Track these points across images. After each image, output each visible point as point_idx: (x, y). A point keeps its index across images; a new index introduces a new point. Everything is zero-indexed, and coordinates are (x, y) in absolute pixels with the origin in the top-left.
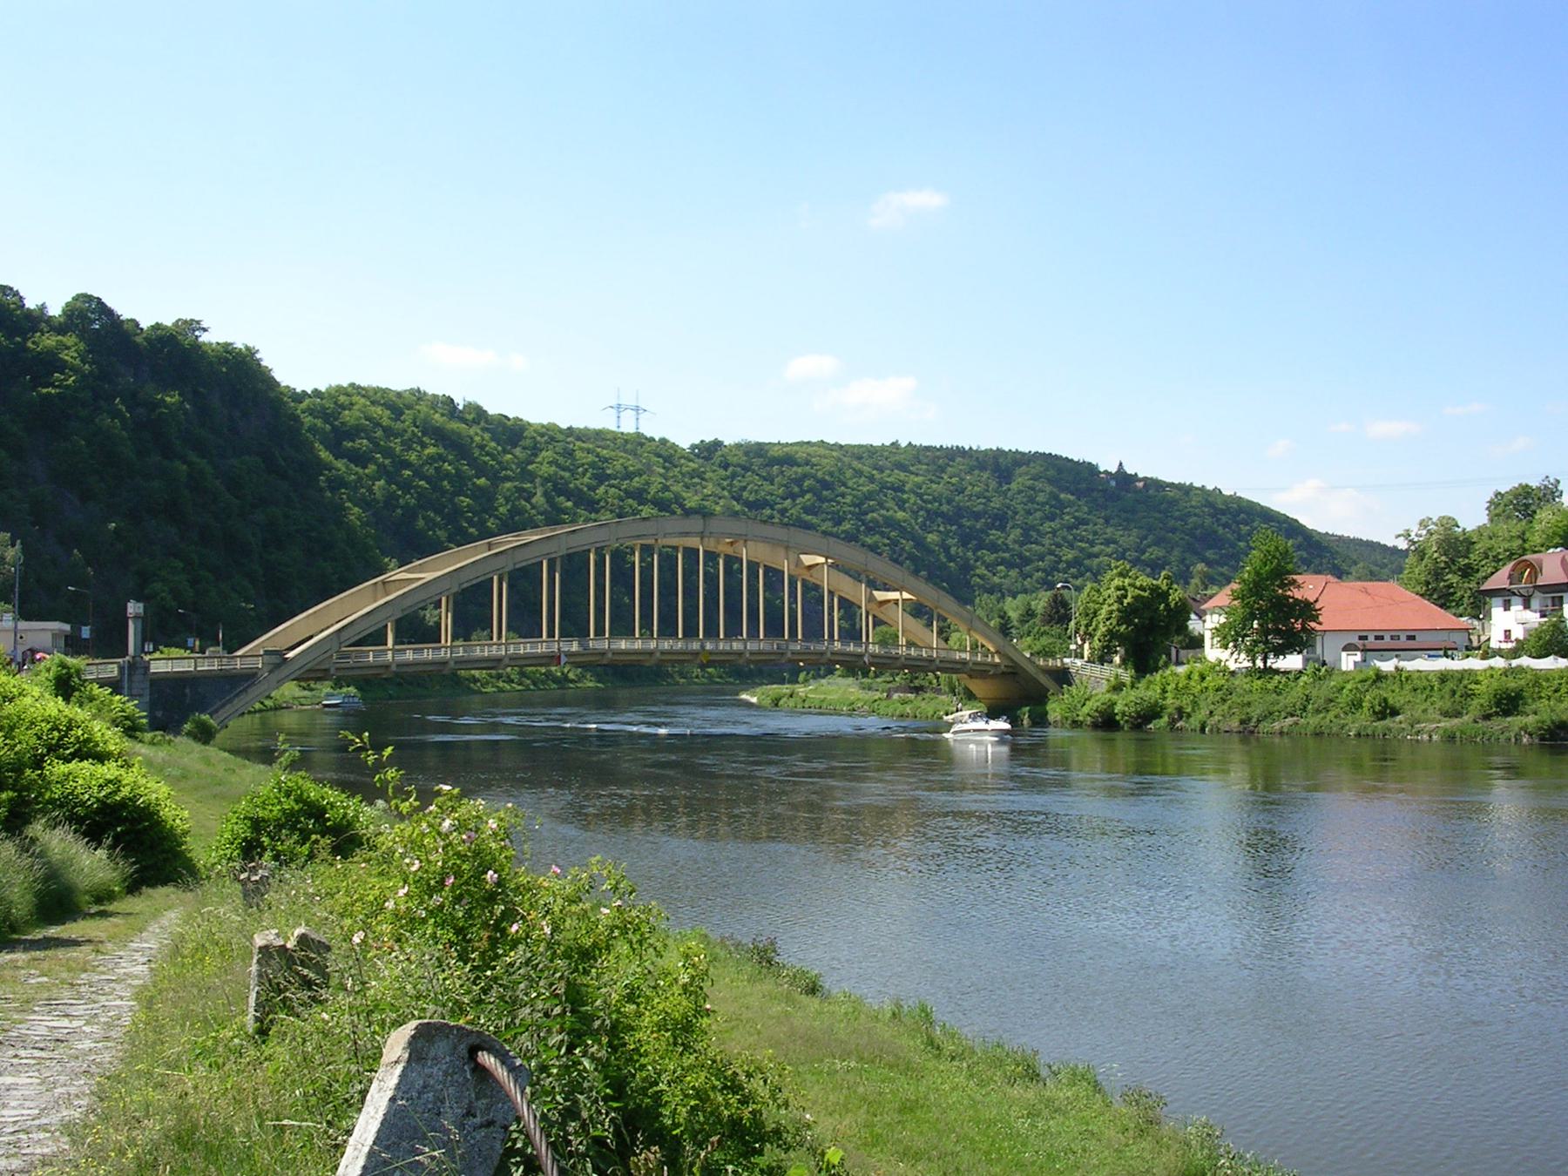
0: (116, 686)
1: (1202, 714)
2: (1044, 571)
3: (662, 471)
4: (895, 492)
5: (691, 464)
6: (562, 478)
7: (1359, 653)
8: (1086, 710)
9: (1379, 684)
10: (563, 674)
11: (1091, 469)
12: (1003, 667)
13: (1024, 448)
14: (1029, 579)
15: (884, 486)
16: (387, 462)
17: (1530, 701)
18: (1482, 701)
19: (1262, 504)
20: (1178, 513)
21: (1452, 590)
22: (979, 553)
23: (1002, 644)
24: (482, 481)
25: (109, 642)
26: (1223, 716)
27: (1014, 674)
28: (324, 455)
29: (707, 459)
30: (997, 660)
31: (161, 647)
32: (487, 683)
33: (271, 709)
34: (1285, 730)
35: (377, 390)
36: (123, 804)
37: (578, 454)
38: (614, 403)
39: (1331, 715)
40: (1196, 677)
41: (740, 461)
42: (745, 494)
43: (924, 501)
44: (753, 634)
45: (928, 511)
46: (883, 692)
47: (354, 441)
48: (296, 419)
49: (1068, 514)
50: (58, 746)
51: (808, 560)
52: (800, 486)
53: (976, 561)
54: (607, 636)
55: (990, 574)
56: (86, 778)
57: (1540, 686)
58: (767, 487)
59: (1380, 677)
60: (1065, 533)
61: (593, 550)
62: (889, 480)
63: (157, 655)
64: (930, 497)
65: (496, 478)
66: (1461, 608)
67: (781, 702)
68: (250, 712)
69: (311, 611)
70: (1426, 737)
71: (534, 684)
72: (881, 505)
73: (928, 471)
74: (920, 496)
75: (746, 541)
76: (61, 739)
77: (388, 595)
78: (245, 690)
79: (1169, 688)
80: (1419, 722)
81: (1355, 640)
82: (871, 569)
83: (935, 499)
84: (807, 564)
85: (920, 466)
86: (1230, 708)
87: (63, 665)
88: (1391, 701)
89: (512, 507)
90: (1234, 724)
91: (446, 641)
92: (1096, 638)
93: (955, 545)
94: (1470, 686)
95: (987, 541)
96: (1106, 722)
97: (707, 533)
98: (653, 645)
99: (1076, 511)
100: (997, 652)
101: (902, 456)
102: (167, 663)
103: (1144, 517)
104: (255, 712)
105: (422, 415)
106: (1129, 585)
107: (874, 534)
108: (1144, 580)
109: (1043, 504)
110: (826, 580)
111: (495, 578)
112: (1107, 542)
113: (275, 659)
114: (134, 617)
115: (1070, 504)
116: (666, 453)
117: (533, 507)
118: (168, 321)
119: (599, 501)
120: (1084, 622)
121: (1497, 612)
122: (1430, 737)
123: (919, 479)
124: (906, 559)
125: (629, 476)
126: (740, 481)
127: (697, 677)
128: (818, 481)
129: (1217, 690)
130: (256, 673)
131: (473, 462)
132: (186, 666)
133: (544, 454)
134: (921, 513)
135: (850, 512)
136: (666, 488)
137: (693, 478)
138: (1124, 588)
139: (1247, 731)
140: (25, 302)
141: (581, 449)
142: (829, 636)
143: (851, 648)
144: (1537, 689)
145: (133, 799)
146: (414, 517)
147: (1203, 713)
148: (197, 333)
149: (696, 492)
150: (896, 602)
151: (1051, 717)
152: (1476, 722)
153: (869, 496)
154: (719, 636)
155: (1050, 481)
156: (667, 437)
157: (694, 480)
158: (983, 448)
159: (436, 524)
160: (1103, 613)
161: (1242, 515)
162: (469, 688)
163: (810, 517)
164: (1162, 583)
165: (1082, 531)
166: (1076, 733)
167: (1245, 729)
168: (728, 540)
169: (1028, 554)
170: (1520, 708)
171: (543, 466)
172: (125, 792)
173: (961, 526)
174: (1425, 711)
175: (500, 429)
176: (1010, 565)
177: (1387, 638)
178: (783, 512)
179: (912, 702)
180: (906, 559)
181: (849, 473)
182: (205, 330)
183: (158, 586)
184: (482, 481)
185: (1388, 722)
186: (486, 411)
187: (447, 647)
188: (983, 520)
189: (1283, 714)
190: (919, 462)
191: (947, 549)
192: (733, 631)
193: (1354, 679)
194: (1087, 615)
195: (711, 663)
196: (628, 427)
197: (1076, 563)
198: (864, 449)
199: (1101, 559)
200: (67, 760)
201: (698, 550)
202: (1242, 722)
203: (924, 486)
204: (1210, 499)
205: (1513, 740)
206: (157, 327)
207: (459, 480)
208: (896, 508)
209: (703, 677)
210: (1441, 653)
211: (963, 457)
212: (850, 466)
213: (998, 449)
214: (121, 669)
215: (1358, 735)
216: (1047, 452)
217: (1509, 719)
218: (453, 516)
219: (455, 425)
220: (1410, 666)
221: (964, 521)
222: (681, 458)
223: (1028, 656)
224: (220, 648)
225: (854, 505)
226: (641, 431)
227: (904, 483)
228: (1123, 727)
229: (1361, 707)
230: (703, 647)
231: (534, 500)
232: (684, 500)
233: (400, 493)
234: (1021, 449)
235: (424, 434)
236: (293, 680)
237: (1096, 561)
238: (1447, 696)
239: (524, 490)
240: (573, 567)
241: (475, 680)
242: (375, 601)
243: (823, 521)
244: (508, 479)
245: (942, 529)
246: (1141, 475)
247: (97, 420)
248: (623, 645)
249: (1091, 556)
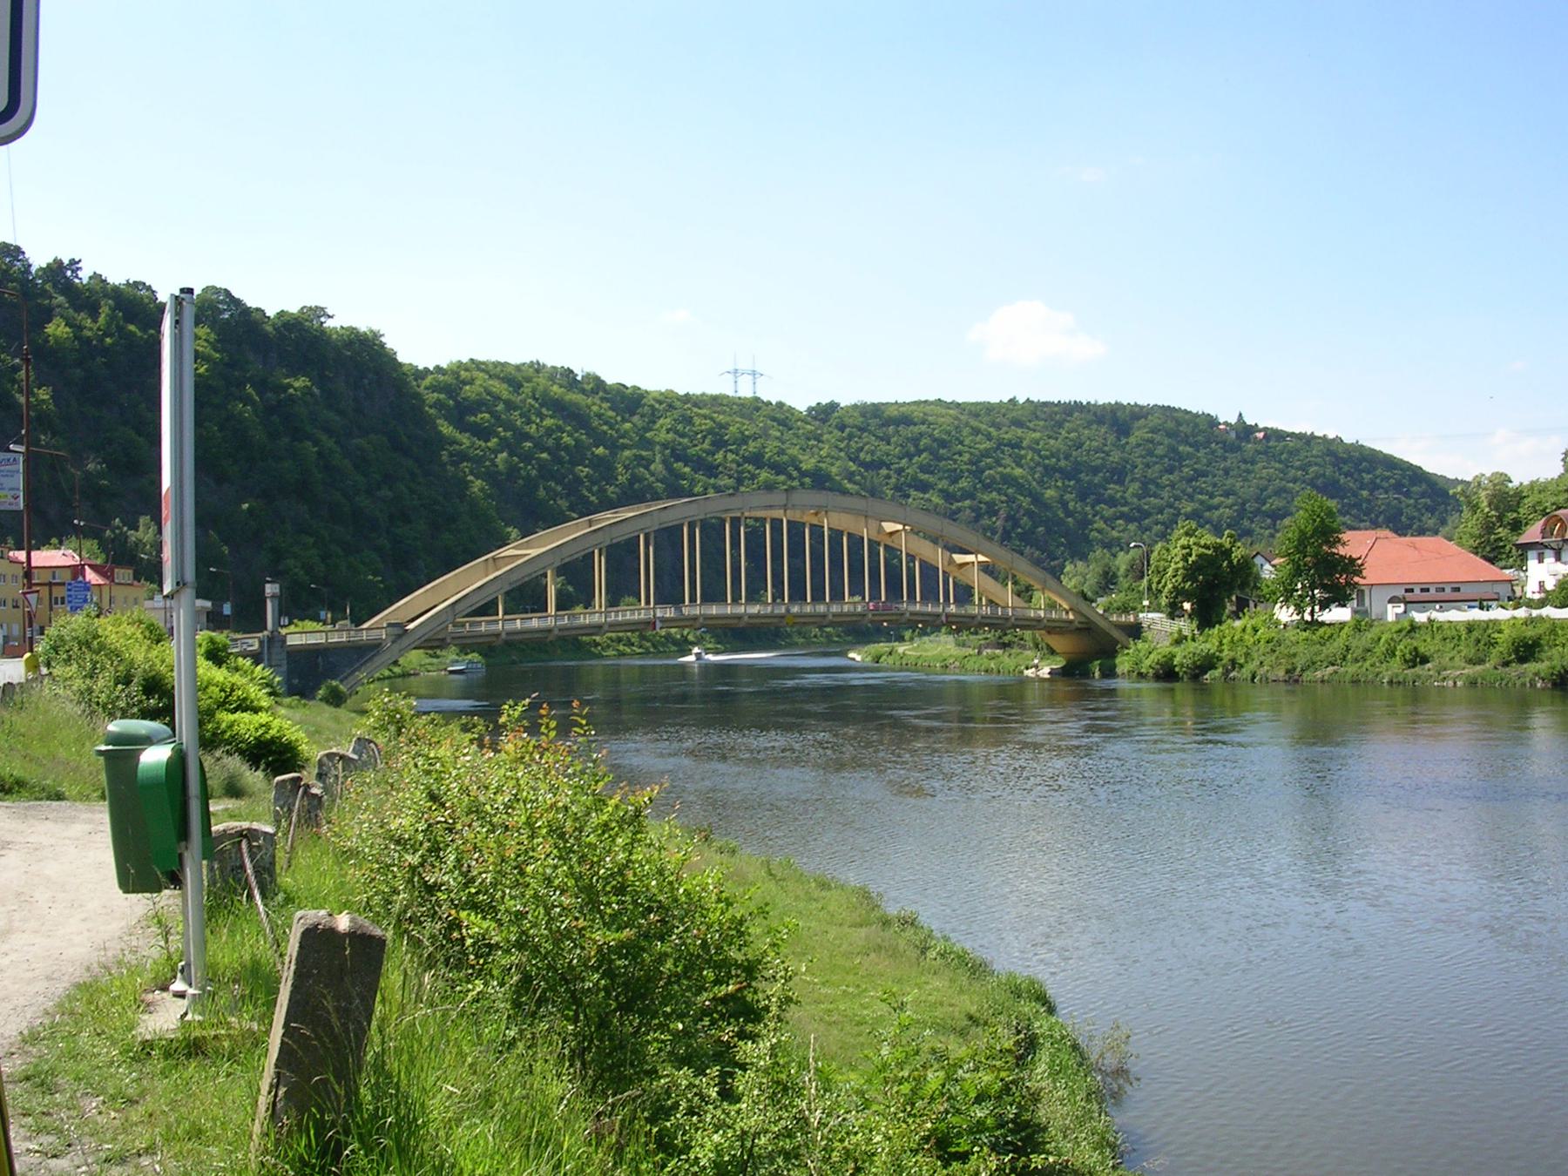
0: (257, 658)
1: (1252, 666)
2: (1163, 523)
3: (778, 434)
5: (809, 427)
6: (680, 444)
7: (1402, 605)
8: (1147, 662)
9: (1413, 634)
10: (682, 636)
11: (1212, 422)
13: (1143, 401)
14: (1148, 533)
15: (1000, 444)
16: (509, 434)
17: (1546, 648)
18: (1501, 649)
19: (1385, 451)
20: (1298, 463)
21: (1501, 544)
22: (1098, 508)
23: (1075, 601)
24: (600, 450)
25: (249, 618)
26: (1271, 666)
27: (1088, 629)
28: (446, 429)
29: (824, 421)
30: (1071, 617)
31: (295, 621)
32: (608, 646)
33: (399, 676)
34: (1326, 678)
35: (497, 364)
36: (273, 740)
37: (697, 421)
38: (731, 369)
39: (1368, 664)
40: (1249, 630)
41: (856, 422)
42: (862, 455)
43: (1041, 457)
44: (736, 599)
45: (1046, 467)
46: (974, 648)
47: (476, 416)
48: (417, 396)
49: (1187, 466)
50: (224, 703)
51: (889, 527)
52: (916, 446)
53: (1094, 516)
54: (698, 602)
55: (1110, 529)
56: (247, 725)
57: (1556, 634)
58: (884, 447)
59: (1414, 628)
60: (1184, 485)
62: (1006, 436)
63: (292, 628)
64: (1048, 453)
65: (614, 447)
66: (1511, 560)
67: (881, 660)
68: (379, 679)
69: (457, 571)
70: (1451, 683)
71: (654, 646)
72: (998, 463)
73: (1045, 427)
74: (1038, 452)
75: (826, 512)
76: (227, 697)
77: (497, 570)
78: (371, 659)
79: (1225, 641)
80: (1445, 670)
81: (1400, 592)
83: (1052, 455)
84: (888, 530)
85: (1037, 422)
86: (1277, 658)
87: (212, 641)
88: (1422, 650)
89: (631, 475)
90: (1281, 673)
91: (601, 607)
92: (1163, 595)
93: (1073, 500)
94: (1493, 636)
95: (1106, 496)
96: (1167, 673)
97: (790, 506)
98: (741, 610)
99: (1195, 463)
100: (1071, 609)
101: (1020, 412)
102: (302, 635)
103: (1264, 468)
104: (384, 679)
105: (541, 388)
106: (1195, 544)
107: (991, 492)
108: (1209, 539)
109: (1162, 457)
110: (903, 544)
111: (596, 551)
112: (1227, 494)
113: (397, 631)
114: (272, 597)
115: (1189, 456)
116: (781, 416)
117: (652, 475)
118: (293, 309)
119: (718, 466)
120: (1156, 580)
121: (1532, 563)
122: (1455, 683)
123: (1037, 435)
124: (1024, 515)
125: (744, 440)
126: (856, 442)
127: (815, 636)
128: (935, 440)
129: (1268, 642)
130: (380, 644)
131: (591, 432)
132: (312, 640)
133: (661, 421)
134: (1039, 469)
136: (782, 452)
137: (809, 439)
138: (1189, 547)
139: (1292, 678)
140: (158, 296)
141: (698, 415)
142: (944, 601)
144: (1552, 637)
145: (280, 738)
146: (536, 487)
147: (1252, 666)
148: (323, 319)
149: (813, 455)
151: (1119, 670)
152: (1496, 668)
153: (986, 454)
154: (806, 600)
155: (1169, 434)
156: (783, 400)
157: (810, 443)
158: (1100, 403)
159: (556, 494)
160: (1170, 572)
161: (1364, 464)
162: (590, 651)
163: (927, 476)
164: (1225, 541)
165: (1201, 483)
166: (1143, 685)
167: (1290, 678)
169: (1146, 507)
170: (1536, 655)
171: (662, 432)
172: (272, 732)
173: (1078, 481)
174: (1452, 659)
175: (619, 398)
176: (1129, 519)
177: (1433, 590)
178: (900, 471)
179: (998, 657)
180: (1024, 515)
181: (966, 431)
182: (330, 317)
183: (291, 562)
184: (600, 450)
185: (1418, 670)
186: (603, 381)
187: (601, 613)
188: (1101, 474)
189: (1325, 664)
190: (1037, 417)
191: (1064, 504)
192: (798, 595)
193: (1390, 629)
194: (1159, 572)
195: (831, 624)
196: (745, 392)
199: (1221, 510)
200: (234, 711)
201: (782, 521)
202: (1288, 671)
203: (1041, 443)
204: (1331, 448)
205: (1528, 685)
206: (281, 314)
207: (578, 454)
208: (1014, 465)
209: (821, 636)
210: (1477, 604)
211: (1081, 412)
212: (967, 424)
213: (1116, 403)
214: (261, 643)
215: (1391, 682)
216: (1166, 405)
217: (1525, 666)
218: (572, 488)
219: (574, 397)
220: (1441, 617)
222: (798, 420)
223: (1101, 612)
224: (348, 622)
225: (971, 462)
226: (758, 395)
227: (1021, 440)
228: (1182, 678)
229: (1394, 655)
230: (788, 610)
231: (652, 467)
232: (801, 462)
233: (522, 465)
234: (1141, 403)
235: (542, 405)
236: (415, 648)
237: (1217, 513)
238: (1471, 645)
239: (642, 458)
240: (668, 539)
241: (597, 644)
242: (487, 576)
243: (940, 479)
244: (625, 447)
245: (1059, 484)
246: (1261, 426)
247: (230, 407)
248: (714, 610)
249: (1210, 508)
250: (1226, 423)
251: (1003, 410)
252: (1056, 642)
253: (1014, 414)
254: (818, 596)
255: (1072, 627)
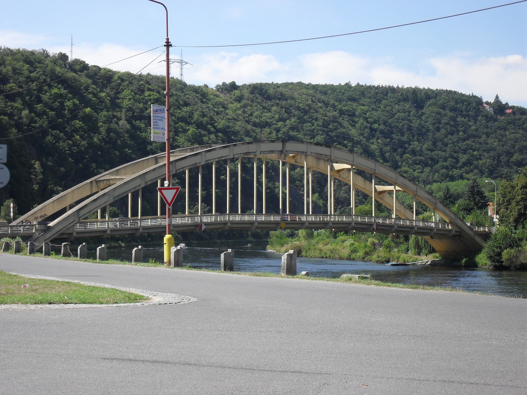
4: (350, 117)
11: (478, 101)
12: (454, 232)
30: (450, 227)
44: (259, 211)
51: (338, 166)
61: (214, 163)
82: (378, 173)
105: (49, 68)
130: (32, 235)
135: (320, 130)
143: (344, 219)
150: (390, 192)
158: (405, 87)
168: (291, 155)
178: (278, 130)
184: (88, 110)
192: (221, 209)
197: (468, 163)
198: (329, 88)
219: (71, 74)
221: (394, 136)
223: (469, 225)
235: (52, 80)
246: (510, 105)
250: (487, 103)
251: (343, 91)
252: (435, 244)
253: (350, 93)
254: (234, 211)
255: (451, 234)
